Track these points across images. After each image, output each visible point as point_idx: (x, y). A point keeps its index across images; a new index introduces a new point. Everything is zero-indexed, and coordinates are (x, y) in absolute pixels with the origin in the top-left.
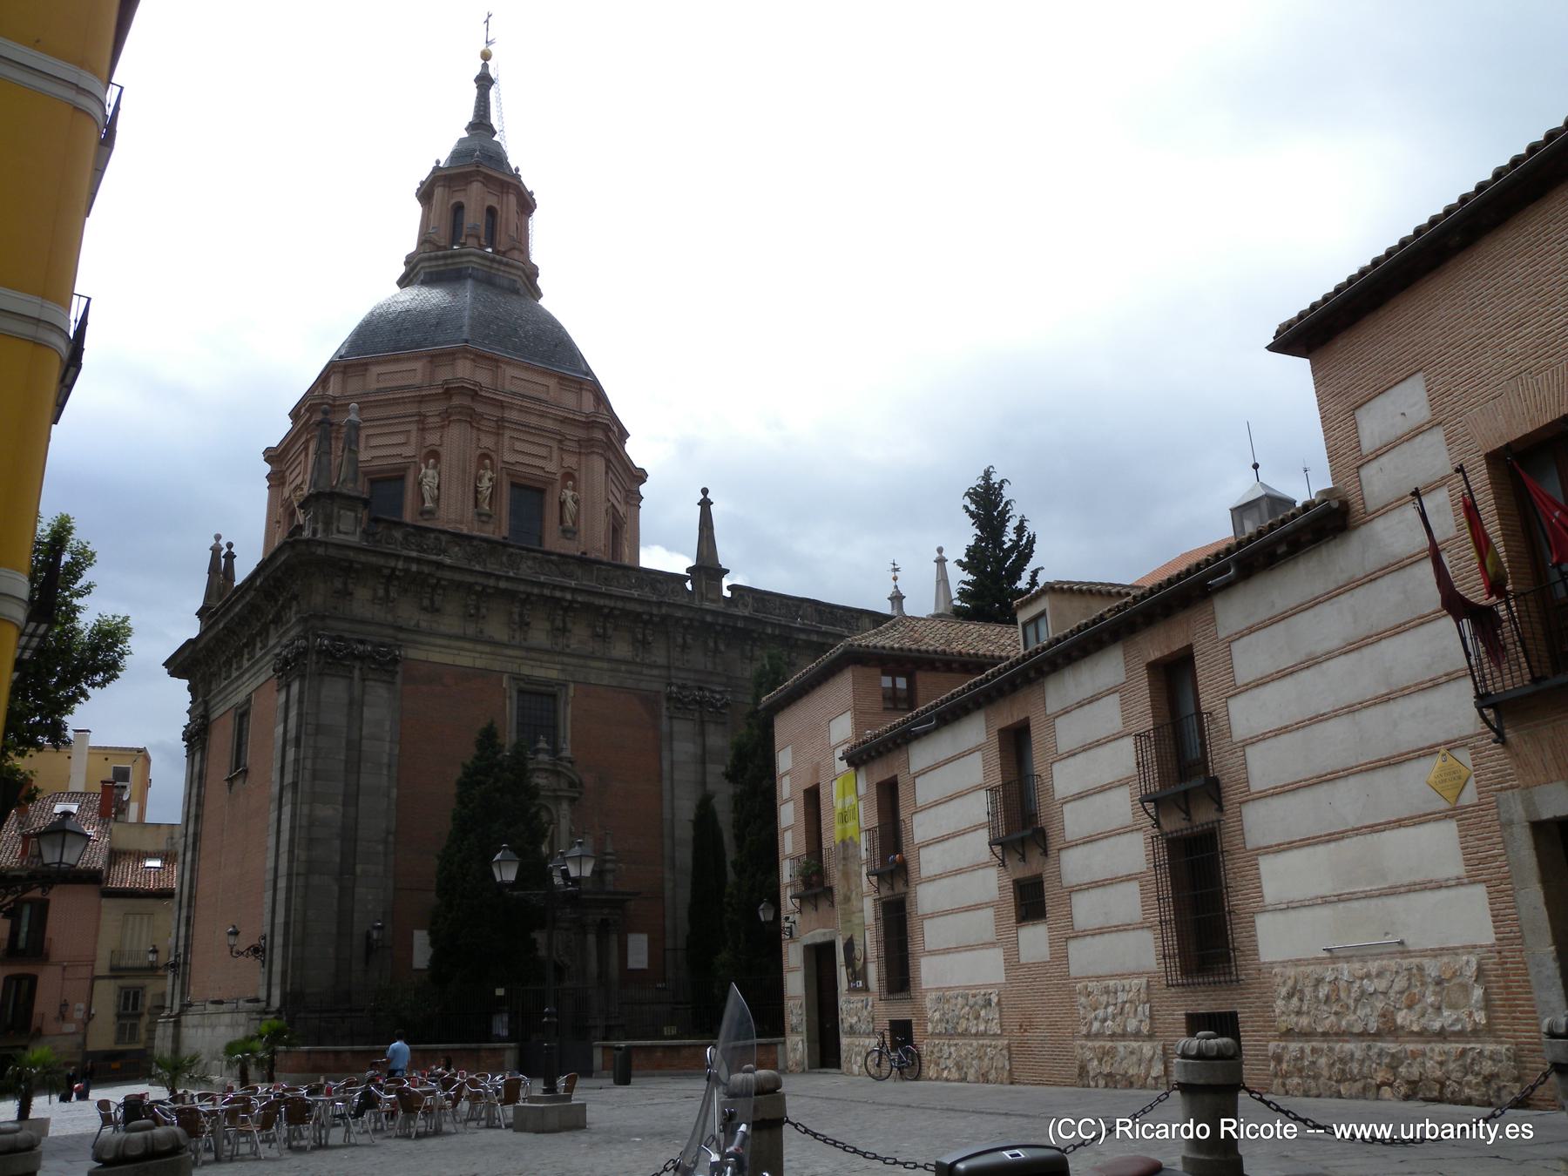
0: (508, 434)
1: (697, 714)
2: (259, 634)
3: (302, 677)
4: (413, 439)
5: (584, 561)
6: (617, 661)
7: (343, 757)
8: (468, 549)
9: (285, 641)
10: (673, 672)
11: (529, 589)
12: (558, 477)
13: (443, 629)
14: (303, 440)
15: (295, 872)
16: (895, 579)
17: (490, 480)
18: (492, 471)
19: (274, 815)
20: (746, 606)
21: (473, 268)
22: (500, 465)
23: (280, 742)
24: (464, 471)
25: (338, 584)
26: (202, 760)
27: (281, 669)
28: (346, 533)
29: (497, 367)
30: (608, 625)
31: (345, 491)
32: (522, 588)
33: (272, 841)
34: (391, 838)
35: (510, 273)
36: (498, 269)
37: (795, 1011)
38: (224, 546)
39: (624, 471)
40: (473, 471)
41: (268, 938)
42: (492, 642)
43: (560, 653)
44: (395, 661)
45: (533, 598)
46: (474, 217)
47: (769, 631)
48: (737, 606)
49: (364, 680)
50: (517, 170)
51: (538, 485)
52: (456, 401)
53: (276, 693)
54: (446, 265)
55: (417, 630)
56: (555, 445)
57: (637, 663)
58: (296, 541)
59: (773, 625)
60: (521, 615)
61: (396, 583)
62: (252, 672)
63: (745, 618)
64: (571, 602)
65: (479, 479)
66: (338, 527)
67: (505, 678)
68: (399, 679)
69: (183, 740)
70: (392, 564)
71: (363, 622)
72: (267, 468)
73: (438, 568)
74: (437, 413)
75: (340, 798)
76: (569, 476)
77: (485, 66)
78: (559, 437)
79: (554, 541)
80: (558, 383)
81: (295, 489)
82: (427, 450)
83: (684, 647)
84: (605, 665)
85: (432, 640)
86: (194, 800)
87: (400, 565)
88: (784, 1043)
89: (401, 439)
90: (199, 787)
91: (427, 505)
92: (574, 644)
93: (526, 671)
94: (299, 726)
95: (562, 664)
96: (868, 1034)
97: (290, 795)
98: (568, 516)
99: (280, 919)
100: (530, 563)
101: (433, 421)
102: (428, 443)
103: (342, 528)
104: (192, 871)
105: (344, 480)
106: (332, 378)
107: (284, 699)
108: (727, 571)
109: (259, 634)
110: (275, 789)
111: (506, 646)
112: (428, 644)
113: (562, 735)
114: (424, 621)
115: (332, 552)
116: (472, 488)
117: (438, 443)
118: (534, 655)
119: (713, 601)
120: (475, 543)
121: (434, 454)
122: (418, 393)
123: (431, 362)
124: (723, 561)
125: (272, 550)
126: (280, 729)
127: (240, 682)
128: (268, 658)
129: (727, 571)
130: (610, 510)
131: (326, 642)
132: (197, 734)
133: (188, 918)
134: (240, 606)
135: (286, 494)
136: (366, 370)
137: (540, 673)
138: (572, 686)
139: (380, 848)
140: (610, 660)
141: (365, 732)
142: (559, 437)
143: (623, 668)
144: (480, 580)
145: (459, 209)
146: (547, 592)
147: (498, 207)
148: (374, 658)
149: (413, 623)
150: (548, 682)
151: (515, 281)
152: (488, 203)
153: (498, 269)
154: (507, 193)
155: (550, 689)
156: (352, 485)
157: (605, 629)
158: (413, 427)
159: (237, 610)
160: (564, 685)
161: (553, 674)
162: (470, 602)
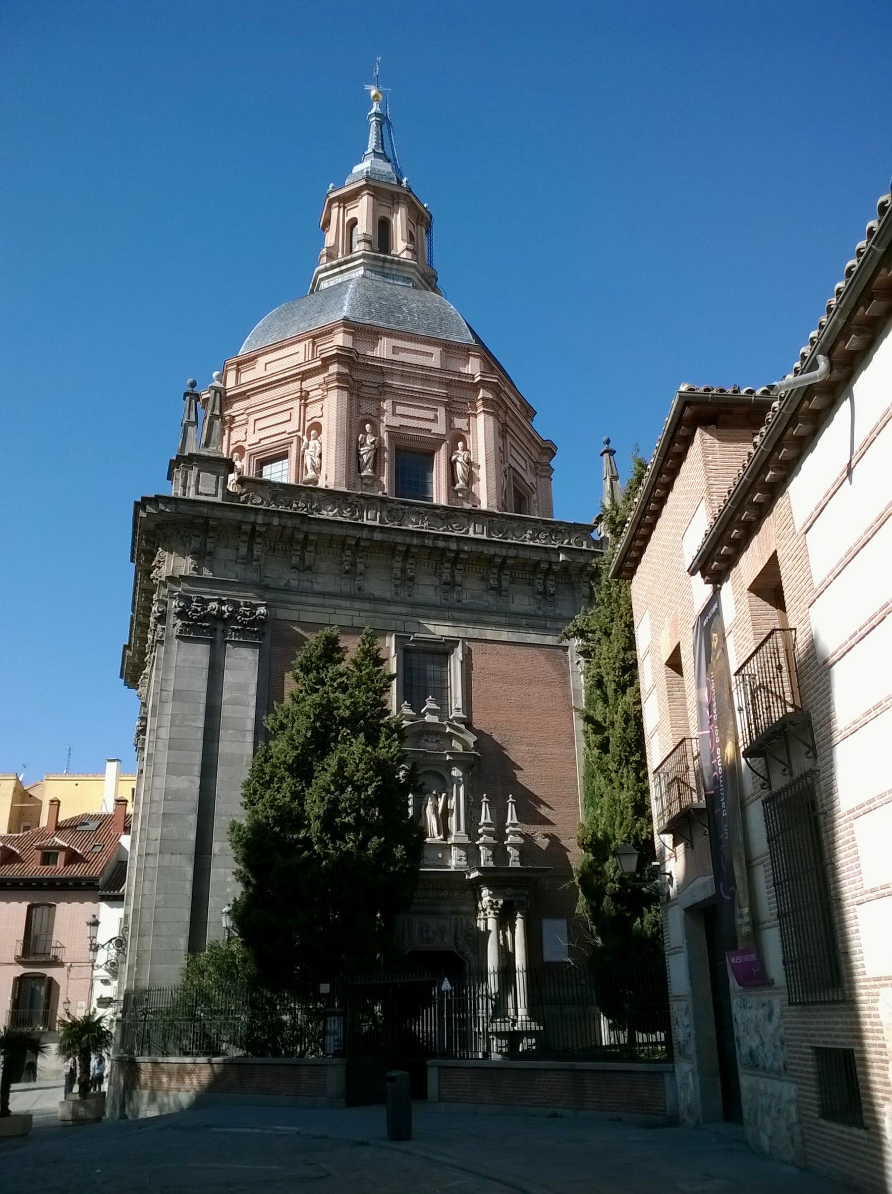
6: (519, 614)
11: (408, 540)
13: (317, 587)
35: (402, 271)
39: (529, 441)
42: (371, 599)
43: (450, 608)
45: (414, 550)
55: (287, 589)
57: (541, 616)
60: (403, 571)
61: (258, 540)
70: (252, 518)
82: (310, 422)
85: (303, 599)
96: (778, 1072)
111: (387, 602)
112: (299, 603)
114: (293, 579)
144: (352, 532)
153: (391, 269)
157: (500, 581)
162: (345, 558)
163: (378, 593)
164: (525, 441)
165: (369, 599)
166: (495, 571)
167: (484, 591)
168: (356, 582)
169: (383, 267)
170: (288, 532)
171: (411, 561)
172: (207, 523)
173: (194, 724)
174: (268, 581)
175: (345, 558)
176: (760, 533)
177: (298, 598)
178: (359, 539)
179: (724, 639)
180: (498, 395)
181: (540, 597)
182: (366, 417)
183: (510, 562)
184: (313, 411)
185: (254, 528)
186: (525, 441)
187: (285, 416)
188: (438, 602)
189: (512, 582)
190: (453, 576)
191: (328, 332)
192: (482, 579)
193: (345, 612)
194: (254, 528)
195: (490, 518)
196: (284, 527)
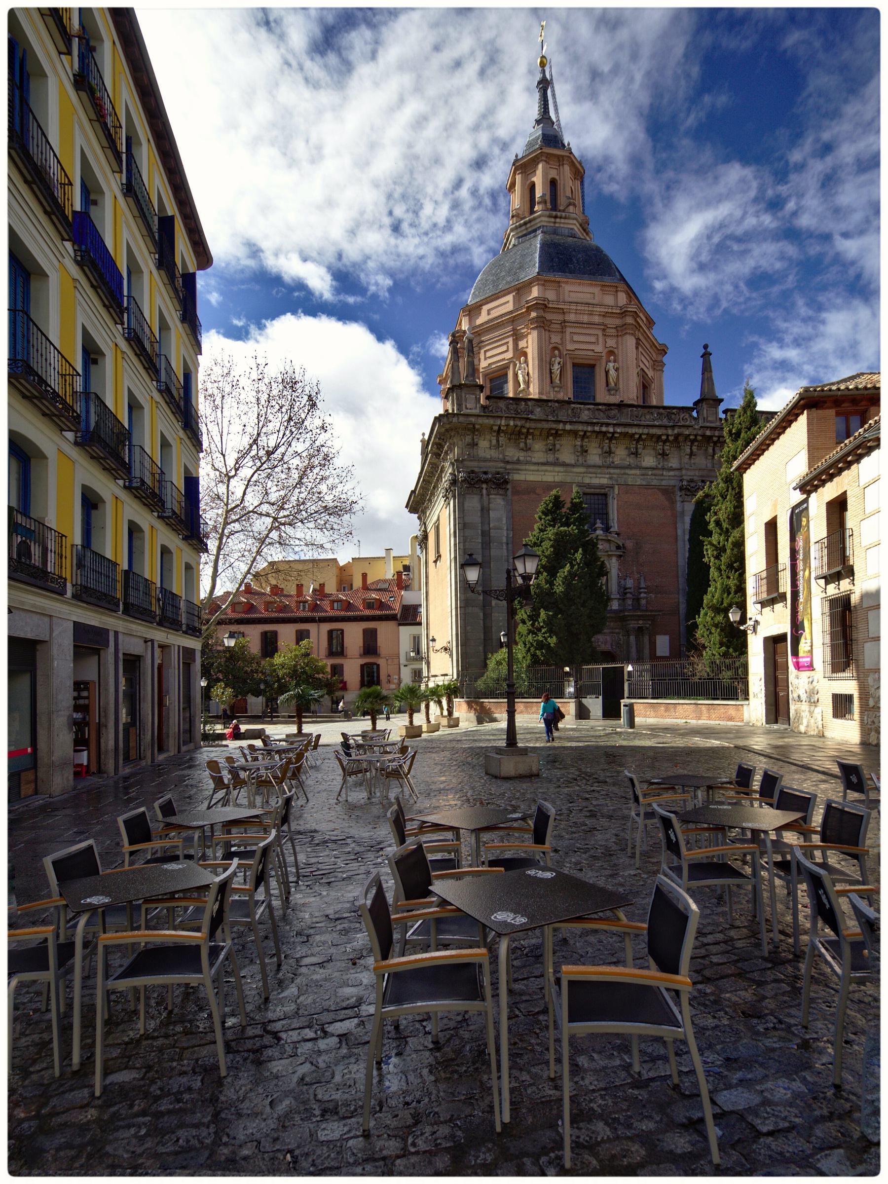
0: (569, 330)
10: (684, 472)
13: (534, 460)
17: (559, 363)
25: (468, 439)
29: (559, 286)
32: (580, 427)
40: (548, 360)
43: (608, 467)
44: (506, 482)
45: (588, 434)
51: (592, 362)
55: (518, 462)
56: (600, 333)
60: (582, 446)
61: (502, 435)
64: (613, 433)
65: (551, 364)
68: (509, 493)
71: (485, 460)
76: (611, 353)
78: (602, 327)
83: (691, 454)
84: (638, 472)
85: (527, 467)
92: (617, 461)
93: (587, 480)
100: (586, 412)
108: (722, 400)
111: (573, 466)
112: (526, 470)
114: (521, 455)
118: (591, 470)
119: (711, 422)
129: (722, 400)
137: (596, 481)
138: (617, 487)
140: (640, 468)
142: (602, 327)
143: (650, 473)
146: (597, 428)
147: (557, 178)
149: (515, 459)
150: (602, 487)
151: (572, 229)
152: (550, 177)
161: (605, 481)
163: (568, 461)
164: (648, 347)
166: (634, 442)
169: (555, 223)
170: (518, 429)
171: (586, 440)
172: (474, 427)
174: (507, 459)
176: (849, 507)
177: (523, 467)
179: (808, 521)
180: (636, 320)
182: (554, 345)
183: (644, 437)
184: (522, 344)
185: (499, 428)
186: (648, 347)
187: (504, 348)
189: (644, 449)
191: (529, 284)
192: (627, 448)
194: (499, 428)
196: (516, 426)
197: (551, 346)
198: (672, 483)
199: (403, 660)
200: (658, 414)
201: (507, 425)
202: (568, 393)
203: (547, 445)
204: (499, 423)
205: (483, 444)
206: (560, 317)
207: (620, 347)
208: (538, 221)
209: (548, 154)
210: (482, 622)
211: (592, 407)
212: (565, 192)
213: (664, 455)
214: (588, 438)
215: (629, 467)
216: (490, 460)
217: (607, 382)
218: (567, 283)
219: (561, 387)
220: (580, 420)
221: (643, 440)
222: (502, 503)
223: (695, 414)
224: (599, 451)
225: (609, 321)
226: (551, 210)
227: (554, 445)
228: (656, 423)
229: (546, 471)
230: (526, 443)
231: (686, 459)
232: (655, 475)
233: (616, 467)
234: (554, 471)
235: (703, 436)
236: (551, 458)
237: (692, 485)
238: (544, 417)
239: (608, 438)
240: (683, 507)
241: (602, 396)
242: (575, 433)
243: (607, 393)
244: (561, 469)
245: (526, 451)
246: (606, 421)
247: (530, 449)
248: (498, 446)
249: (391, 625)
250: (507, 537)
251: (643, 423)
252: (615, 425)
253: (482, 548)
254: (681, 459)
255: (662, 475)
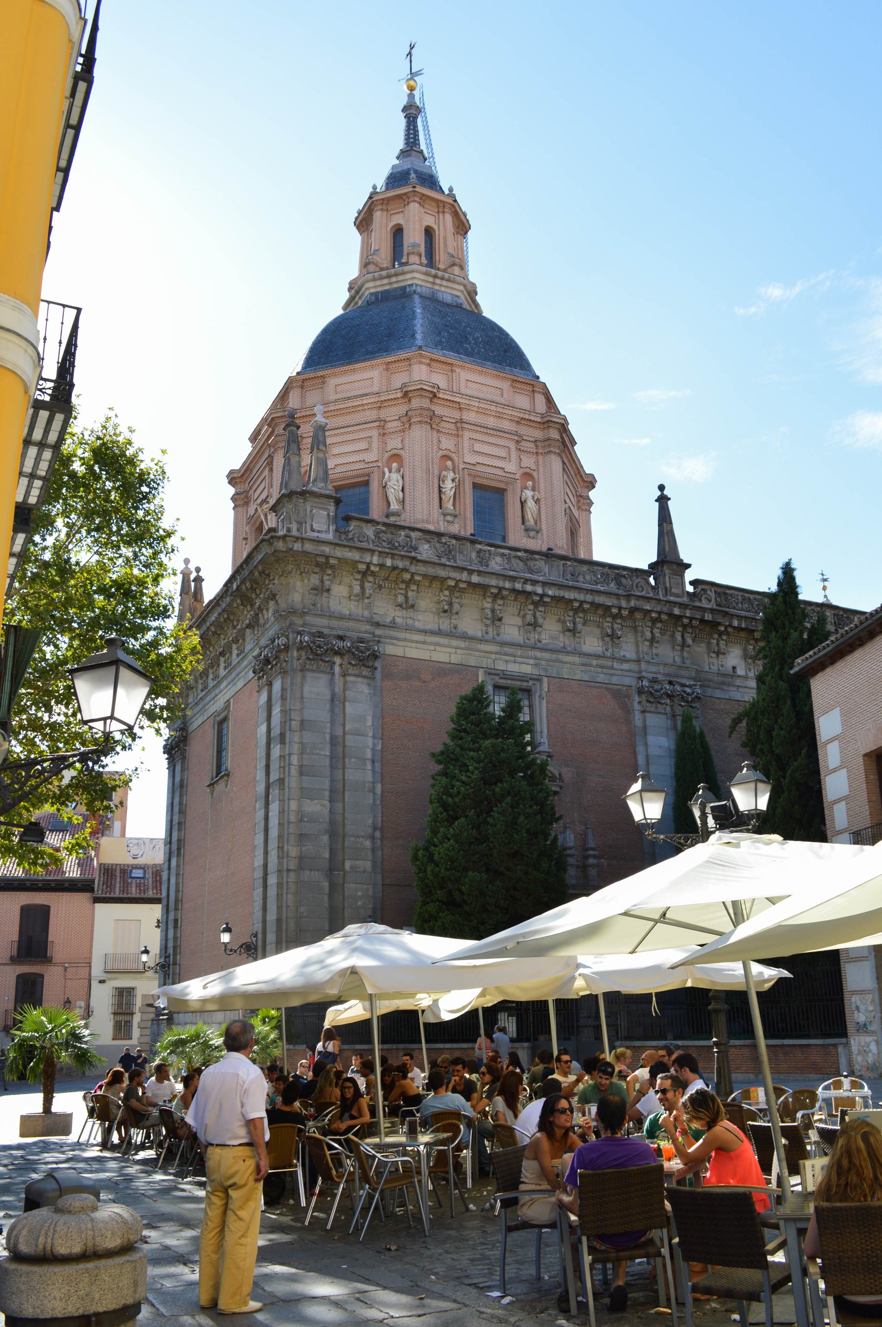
0: (467, 435)
1: (668, 709)
2: (236, 641)
3: (284, 673)
4: (375, 445)
5: (549, 555)
6: (590, 655)
7: (328, 753)
8: (438, 545)
9: (264, 641)
10: (643, 666)
12: (518, 476)
13: (418, 625)
14: (266, 455)
15: (285, 868)
16: (824, 588)
17: (453, 480)
18: (454, 472)
19: (261, 814)
20: (710, 601)
21: (417, 285)
22: (462, 466)
23: (264, 741)
24: (428, 471)
25: (315, 580)
26: (182, 770)
27: (262, 670)
28: (319, 532)
29: (452, 371)
30: (578, 620)
31: (315, 489)
32: (493, 582)
33: (259, 839)
34: (378, 834)
36: (441, 285)
37: (862, 1008)
38: (193, 569)
40: (436, 472)
41: (260, 936)
42: (464, 637)
43: (534, 648)
44: (375, 656)
45: (505, 593)
46: (414, 237)
47: (736, 623)
48: (701, 600)
49: (344, 675)
50: (451, 190)
51: (502, 486)
52: (416, 403)
53: (256, 694)
54: (390, 284)
55: (393, 625)
56: (512, 446)
58: (272, 537)
59: (740, 618)
60: (493, 611)
61: (371, 579)
62: (230, 679)
63: (712, 610)
64: (542, 596)
65: (441, 479)
66: (312, 525)
67: (481, 673)
68: (378, 674)
69: (164, 753)
71: (342, 618)
72: (231, 491)
73: (411, 563)
74: (397, 418)
75: (327, 793)
76: (528, 476)
77: (411, 96)
78: (516, 438)
79: (516, 537)
80: (511, 386)
81: (261, 504)
83: (653, 640)
84: (577, 659)
85: (408, 636)
86: (176, 809)
87: (375, 559)
88: (847, 1045)
89: (363, 445)
90: (181, 796)
91: (392, 507)
92: (545, 639)
93: (501, 666)
94: (283, 723)
95: (536, 658)
97: (277, 791)
98: (530, 516)
99: (272, 916)
100: (498, 559)
101: (392, 426)
102: (389, 448)
103: (315, 526)
104: (178, 875)
105: (315, 480)
106: (291, 394)
107: (266, 699)
108: (688, 566)
109: (236, 641)
110: (261, 788)
111: (481, 641)
112: (405, 640)
113: (539, 730)
114: (400, 616)
115: (309, 547)
116: (436, 486)
117: (400, 446)
118: (507, 649)
119: (677, 596)
120: (444, 540)
121: (396, 457)
122: (377, 399)
123: (387, 369)
124: (685, 555)
125: (238, 564)
126: (263, 728)
127: (217, 691)
128: (245, 663)
129: (688, 566)
130: (568, 510)
131: (306, 638)
132: (177, 745)
133: (176, 921)
134: (216, 615)
135: (251, 511)
136: (323, 383)
137: (514, 668)
138: (545, 680)
139: (368, 843)
140: (581, 654)
141: (348, 727)
142: (516, 438)
143: (594, 662)
145: (398, 232)
146: (518, 586)
147: (435, 227)
148: (353, 653)
149: (389, 620)
150: (523, 678)
151: (457, 296)
152: (425, 224)
153: (441, 285)
154: (444, 212)
155: (525, 684)
156: (323, 485)
158: (374, 433)
159: (213, 618)
160: (539, 680)
161: (527, 669)
163: (471, 632)
165: (464, 637)
166: (571, 613)
167: (560, 632)
168: (453, 621)
171: (500, 602)
172: (327, 562)
173: (322, 753)
174: (377, 618)
175: (443, 598)
177: (402, 635)
178: (458, 581)
181: (607, 639)
182: (446, 453)
188: (522, 642)
190: (535, 617)
192: (559, 620)
193: (444, 649)
195: (563, 562)
197: (441, 453)
198: (627, 681)
199: (97, 971)
200: (602, 574)
201: (382, 566)
202: (466, 526)
203: (439, 602)
204: (368, 560)
205: (339, 590)
206: (456, 415)
207: (541, 470)
208: (408, 276)
209: (424, 195)
210: (326, 898)
211: (507, 552)
212: (446, 246)
213: (613, 637)
214: (503, 598)
215: (563, 650)
216: (350, 618)
217: (523, 517)
218: (463, 367)
219: (455, 516)
220: (489, 570)
221: (584, 611)
222: (366, 691)
223: (652, 580)
224: (519, 621)
225: (524, 430)
226: (426, 266)
227: (451, 604)
228: (599, 587)
229: (438, 644)
230: (406, 597)
231: (645, 647)
232: (602, 667)
233: (543, 649)
234: (449, 646)
235: (670, 615)
236: (445, 625)
237: (657, 687)
238: (435, 559)
239: (533, 603)
240: (644, 722)
241: (516, 537)
242: (483, 588)
243: (523, 533)
244: (462, 644)
245: (407, 608)
246: (528, 576)
247: (413, 606)
248: (362, 595)
249: (80, 900)
250: (373, 750)
251: (580, 585)
252: (544, 584)
253: (331, 767)
254: (637, 646)
255: (612, 668)
